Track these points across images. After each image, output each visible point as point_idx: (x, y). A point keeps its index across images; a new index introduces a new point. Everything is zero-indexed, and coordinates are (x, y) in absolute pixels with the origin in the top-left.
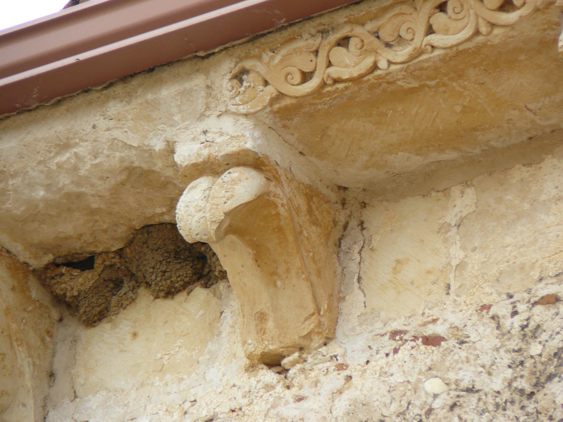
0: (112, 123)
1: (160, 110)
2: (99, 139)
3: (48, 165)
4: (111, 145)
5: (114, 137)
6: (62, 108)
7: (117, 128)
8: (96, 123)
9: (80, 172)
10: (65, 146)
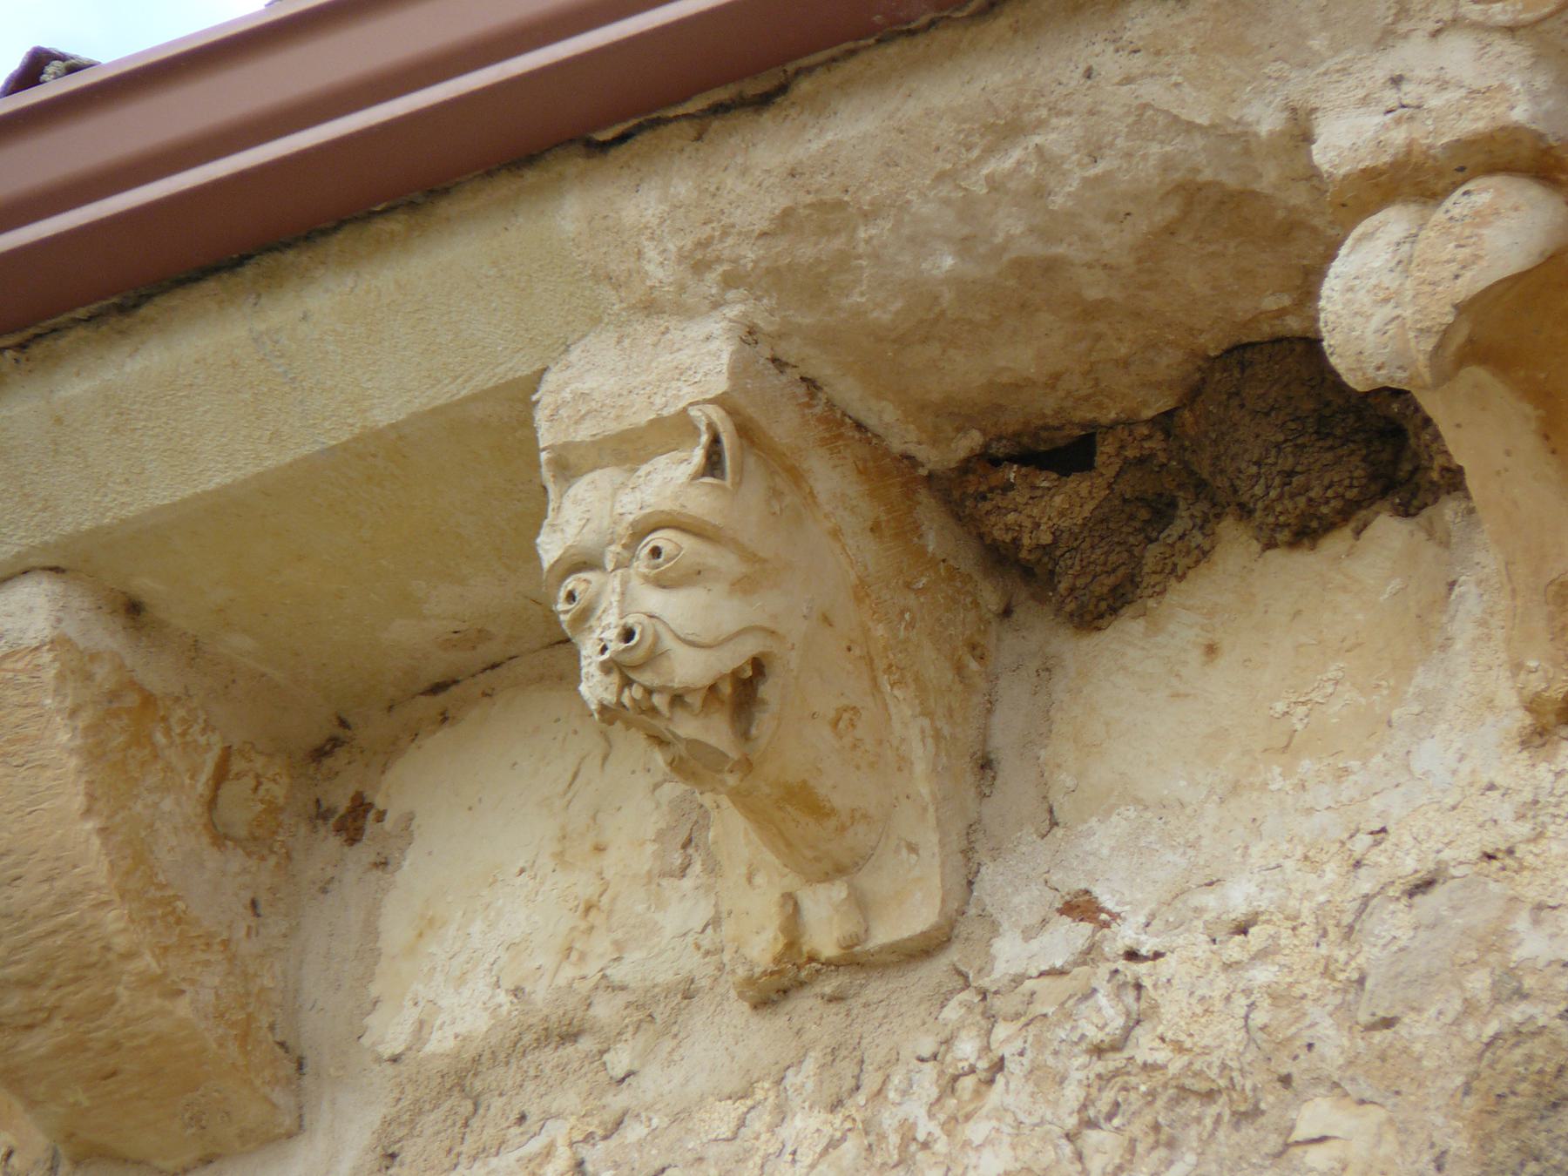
0: (1138, 63)
2: (1104, 108)
5: (1143, 101)
7: (1152, 75)
8: (1093, 62)
9: (1053, 202)
10: (1009, 130)
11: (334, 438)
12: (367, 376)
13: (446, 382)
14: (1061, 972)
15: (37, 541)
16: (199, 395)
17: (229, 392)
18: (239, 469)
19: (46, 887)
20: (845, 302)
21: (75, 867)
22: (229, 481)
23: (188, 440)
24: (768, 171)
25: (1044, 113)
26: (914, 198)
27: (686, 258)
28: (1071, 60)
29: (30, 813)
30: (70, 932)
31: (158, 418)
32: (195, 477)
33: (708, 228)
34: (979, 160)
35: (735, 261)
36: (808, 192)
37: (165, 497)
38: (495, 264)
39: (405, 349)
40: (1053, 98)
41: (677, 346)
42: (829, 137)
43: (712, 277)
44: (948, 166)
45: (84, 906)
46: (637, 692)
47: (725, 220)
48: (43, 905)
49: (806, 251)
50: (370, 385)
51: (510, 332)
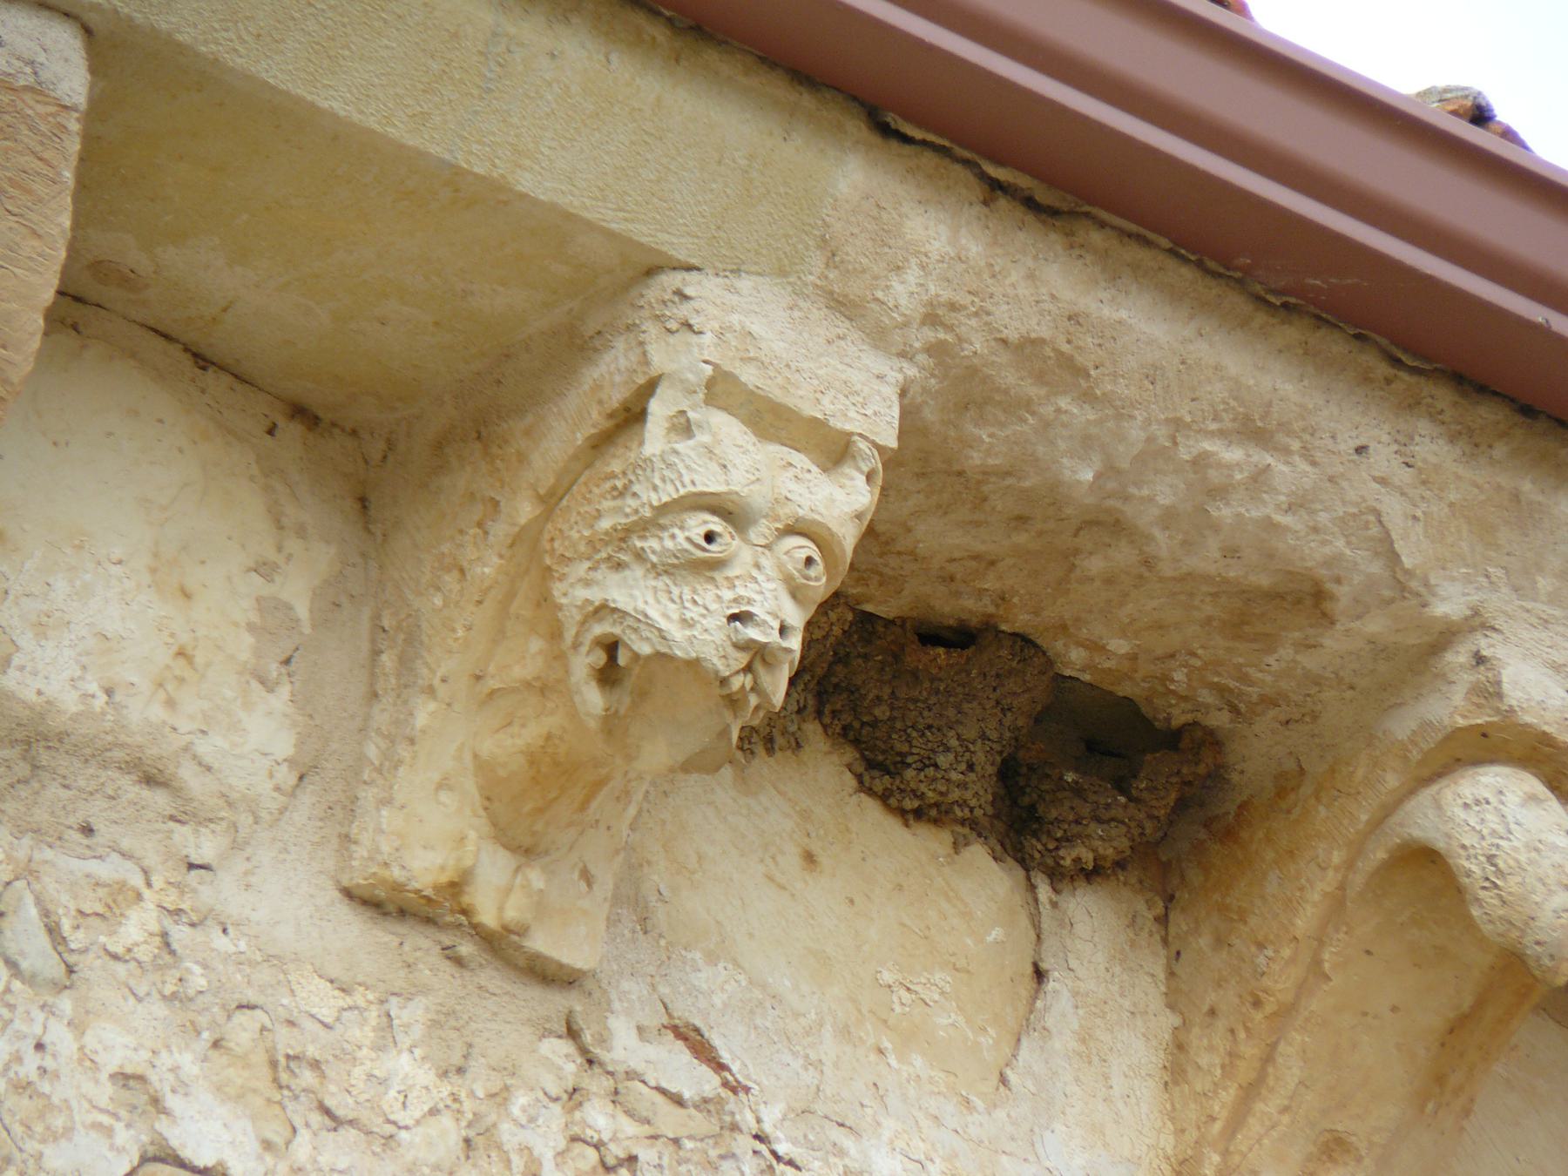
0: (1404, 476)
1: (1527, 536)
2: (1345, 484)
3: (1179, 439)
5: (1378, 506)
6: (1291, 333)
7: (1403, 494)
8: (1373, 445)
9: (1219, 509)
10: (1253, 432)
11: (468, 162)
12: (554, 144)
13: (610, 205)
14: (678, 1101)
15: (126, 10)
16: (398, 30)
17: (424, 50)
18: (361, 112)
22: (342, 113)
23: (347, 53)
24: (1053, 296)
25: (1296, 445)
26: (1139, 418)
27: (932, 304)
28: (1357, 428)
31: (342, 15)
32: (318, 85)
33: (971, 298)
34: (1211, 434)
35: (960, 339)
36: (1069, 342)
37: (275, 77)
39: (608, 153)
40: (1317, 443)
41: (847, 360)
42: (1123, 314)
43: (930, 335)
44: (1188, 419)
46: (748, 680)
47: (988, 305)
49: (1009, 377)
50: (546, 151)
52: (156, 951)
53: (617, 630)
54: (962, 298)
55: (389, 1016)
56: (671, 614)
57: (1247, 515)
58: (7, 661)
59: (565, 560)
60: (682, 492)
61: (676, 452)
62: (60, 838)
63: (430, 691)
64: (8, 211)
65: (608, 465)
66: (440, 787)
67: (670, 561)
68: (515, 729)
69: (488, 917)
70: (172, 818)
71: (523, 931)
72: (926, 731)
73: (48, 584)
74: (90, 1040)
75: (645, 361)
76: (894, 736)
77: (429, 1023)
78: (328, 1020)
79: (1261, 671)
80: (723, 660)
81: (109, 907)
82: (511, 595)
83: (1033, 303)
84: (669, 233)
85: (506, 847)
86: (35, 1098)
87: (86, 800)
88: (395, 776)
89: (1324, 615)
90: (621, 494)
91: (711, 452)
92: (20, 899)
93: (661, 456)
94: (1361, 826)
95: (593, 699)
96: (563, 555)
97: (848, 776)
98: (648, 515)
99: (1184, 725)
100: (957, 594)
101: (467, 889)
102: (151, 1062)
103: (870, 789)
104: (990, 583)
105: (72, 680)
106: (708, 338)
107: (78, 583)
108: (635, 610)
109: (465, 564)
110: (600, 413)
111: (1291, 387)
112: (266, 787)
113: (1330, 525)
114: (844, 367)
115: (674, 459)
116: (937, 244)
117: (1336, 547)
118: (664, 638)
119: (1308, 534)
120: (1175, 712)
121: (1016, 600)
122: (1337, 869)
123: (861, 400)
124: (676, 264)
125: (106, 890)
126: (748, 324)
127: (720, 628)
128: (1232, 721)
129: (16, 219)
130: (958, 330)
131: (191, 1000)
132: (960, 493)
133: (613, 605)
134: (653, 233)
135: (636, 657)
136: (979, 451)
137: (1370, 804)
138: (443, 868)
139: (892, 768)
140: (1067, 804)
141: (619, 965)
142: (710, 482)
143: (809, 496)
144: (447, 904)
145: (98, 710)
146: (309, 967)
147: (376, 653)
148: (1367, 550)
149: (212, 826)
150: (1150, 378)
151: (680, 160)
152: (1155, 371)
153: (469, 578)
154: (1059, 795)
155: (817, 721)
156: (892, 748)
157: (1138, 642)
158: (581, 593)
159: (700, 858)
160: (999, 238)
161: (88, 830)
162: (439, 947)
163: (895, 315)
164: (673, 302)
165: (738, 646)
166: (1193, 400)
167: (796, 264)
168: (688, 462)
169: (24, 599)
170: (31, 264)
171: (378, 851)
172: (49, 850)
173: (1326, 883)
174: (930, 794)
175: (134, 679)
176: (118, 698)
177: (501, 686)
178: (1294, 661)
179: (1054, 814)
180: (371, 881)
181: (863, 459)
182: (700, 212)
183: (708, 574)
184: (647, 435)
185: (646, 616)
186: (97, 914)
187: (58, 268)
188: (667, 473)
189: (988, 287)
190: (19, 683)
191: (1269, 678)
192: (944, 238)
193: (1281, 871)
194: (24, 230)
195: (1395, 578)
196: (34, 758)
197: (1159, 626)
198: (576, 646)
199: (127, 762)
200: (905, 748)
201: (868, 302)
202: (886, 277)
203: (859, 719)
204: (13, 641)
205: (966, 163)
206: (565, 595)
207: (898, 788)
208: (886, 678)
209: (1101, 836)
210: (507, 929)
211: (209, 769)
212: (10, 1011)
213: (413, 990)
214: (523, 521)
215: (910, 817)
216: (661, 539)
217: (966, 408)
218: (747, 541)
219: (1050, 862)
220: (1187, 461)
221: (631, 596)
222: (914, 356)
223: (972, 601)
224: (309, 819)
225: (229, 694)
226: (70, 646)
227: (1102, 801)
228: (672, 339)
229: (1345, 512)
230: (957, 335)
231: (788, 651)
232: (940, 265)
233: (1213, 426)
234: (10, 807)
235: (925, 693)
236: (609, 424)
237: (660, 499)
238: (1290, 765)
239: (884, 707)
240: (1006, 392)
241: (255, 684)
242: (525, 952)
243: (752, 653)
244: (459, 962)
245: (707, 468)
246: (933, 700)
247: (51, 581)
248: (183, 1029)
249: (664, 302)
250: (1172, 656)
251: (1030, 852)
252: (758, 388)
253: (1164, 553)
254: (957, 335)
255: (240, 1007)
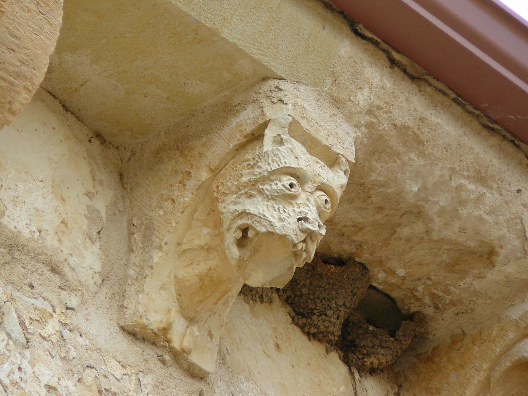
2: (511, 205)
3: (453, 177)
4: (512, 219)
5: (522, 216)
6: (495, 140)
8: (523, 190)
12: (238, 18)
13: (255, 47)
19: (19, 64)
20: (374, 163)
21: (34, 69)
24: (415, 109)
25: (495, 186)
27: (371, 105)
29: (36, 34)
30: (9, 86)
33: (385, 105)
34: (464, 177)
35: (379, 122)
36: (418, 129)
38: (310, 34)
43: (369, 119)
45: (23, 83)
46: (304, 246)
48: (12, 68)
49: (394, 142)
51: (289, 57)
52: (59, 339)
53: (250, 222)
54: (383, 105)
55: (139, 380)
56: (275, 216)
57: (473, 214)
58: (4, 213)
59: (225, 194)
60: (281, 166)
61: (278, 150)
62: (21, 288)
63: (160, 248)
64: (40, 12)
65: (244, 156)
66: (161, 288)
67: (274, 194)
68: (194, 266)
69: (176, 345)
70: (60, 287)
71: (188, 352)
72: (323, 300)
73: (16, 185)
74: (36, 369)
75: (263, 113)
76: (309, 301)
77: (154, 385)
78: (119, 378)
79: (456, 288)
80: (296, 236)
81: (41, 318)
82: (195, 210)
83: (408, 111)
84: (275, 62)
85: (184, 317)
86: (19, 389)
87: (31, 274)
88: (144, 281)
89: (491, 263)
90: (252, 167)
91: (292, 151)
92: (10, 309)
93: (272, 151)
94: (497, 353)
95: (235, 252)
96: (223, 192)
97: (289, 317)
98: (266, 175)
99: (415, 312)
100: (342, 243)
101: (169, 332)
102: (58, 383)
103: (297, 323)
104: (358, 238)
105: (26, 225)
106: (290, 106)
107: (27, 187)
108: (259, 213)
109: (174, 197)
110: (240, 135)
111: (496, 161)
112: (91, 282)
113: (503, 222)
114: (336, 127)
115: (277, 152)
116: (376, 80)
117: (504, 232)
118: (272, 225)
119: (494, 225)
120: (412, 306)
121: (366, 247)
122: (485, 371)
123: (342, 142)
124: (276, 77)
125: (39, 311)
126: (303, 103)
127: (295, 223)
128: (434, 312)
129: (43, 16)
130: (379, 118)
131: (71, 360)
132: (360, 193)
133: (248, 212)
134: (269, 61)
135: (258, 233)
136: (376, 173)
137: (501, 345)
138: (161, 322)
139: (306, 315)
140: (369, 340)
141: (216, 375)
142: (293, 164)
143: (326, 175)
144: (162, 337)
145: (36, 238)
146: (111, 355)
147: (131, 234)
148: (515, 235)
149: (75, 292)
150: (446, 149)
151: (283, 31)
152: (448, 146)
153: (177, 202)
154: (366, 336)
155: (277, 293)
156: (307, 306)
157: (409, 271)
158: (232, 207)
159: (240, 339)
160: (396, 82)
161: (32, 286)
162: (157, 355)
163: (357, 108)
164: (275, 91)
165: (302, 231)
166: (460, 161)
167: (321, 82)
168: (283, 154)
169: (8, 189)
170: (47, 35)
171: (138, 311)
172: (18, 292)
173: (480, 377)
174: (322, 327)
175: (48, 228)
176: (43, 235)
177: (189, 248)
178: (472, 284)
179: (364, 343)
180: (134, 323)
181: (343, 165)
182: (288, 55)
183: (290, 201)
184: (264, 143)
185: (264, 216)
186: (37, 320)
187: (56, 38)
188: (274, 158)
189: (392, 101)
190: (8, 222)
191: (458, 292)
192: (378, 78)
193: (457, 372)
194: (45, 21)
195: (523, 248)
196: (12, 254)
197: (420, 264)
198: (228, 229)
199: (46, 261)
200: (314, 307)
201: (347, 101)
202: (355, 91)
203: (294, 294)
204: (5, 205)
205: (383, 50)
206: (224, 208)
207: (309, 324)
208: (308, 276)
209: (382, 354)
210: (183, 351)
211: (74, 270)
212: (9, 352)
213: (148, 371)
214: (203, 179)
215: (312, 336)
216: (271, 185)
217: (374, 154)
218: (303, 190)
219: (360, 363)
220: (454, 187)
221: (257, 208)
222: (360, 127)
223: (347, 246)
224: (105, 298)
225: (79, 241)
226: (25, 211)
227: (384, 339)
228: (274, 106)
229: (509, 217)
230: (378, 120)
231: (321, 234)
232: (376, 89)
233: (466, 173)
234: (3, 273)
235: (324, 284)
236: (244, 140)
237: (271, 169)
238: (459, 331)
239: (306, 289)
240: (391, 148)
241: (88, 240)
242: (188, 362)
243: (307, 234)
244: (164, 362)
245: (290, 157)
246: (327, 287)
247: (18, 184)
248: (68, 372)
249: (271, 91)
250: (419, 279)
251: (351, 359)
252: (307, 129)
253: (436, 228)
254: (378, 120)
255: (87, 367)
